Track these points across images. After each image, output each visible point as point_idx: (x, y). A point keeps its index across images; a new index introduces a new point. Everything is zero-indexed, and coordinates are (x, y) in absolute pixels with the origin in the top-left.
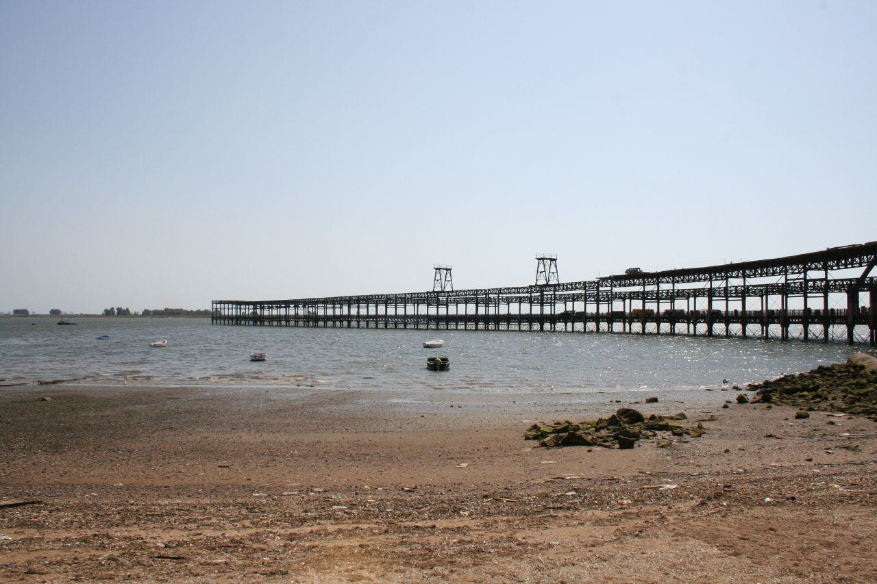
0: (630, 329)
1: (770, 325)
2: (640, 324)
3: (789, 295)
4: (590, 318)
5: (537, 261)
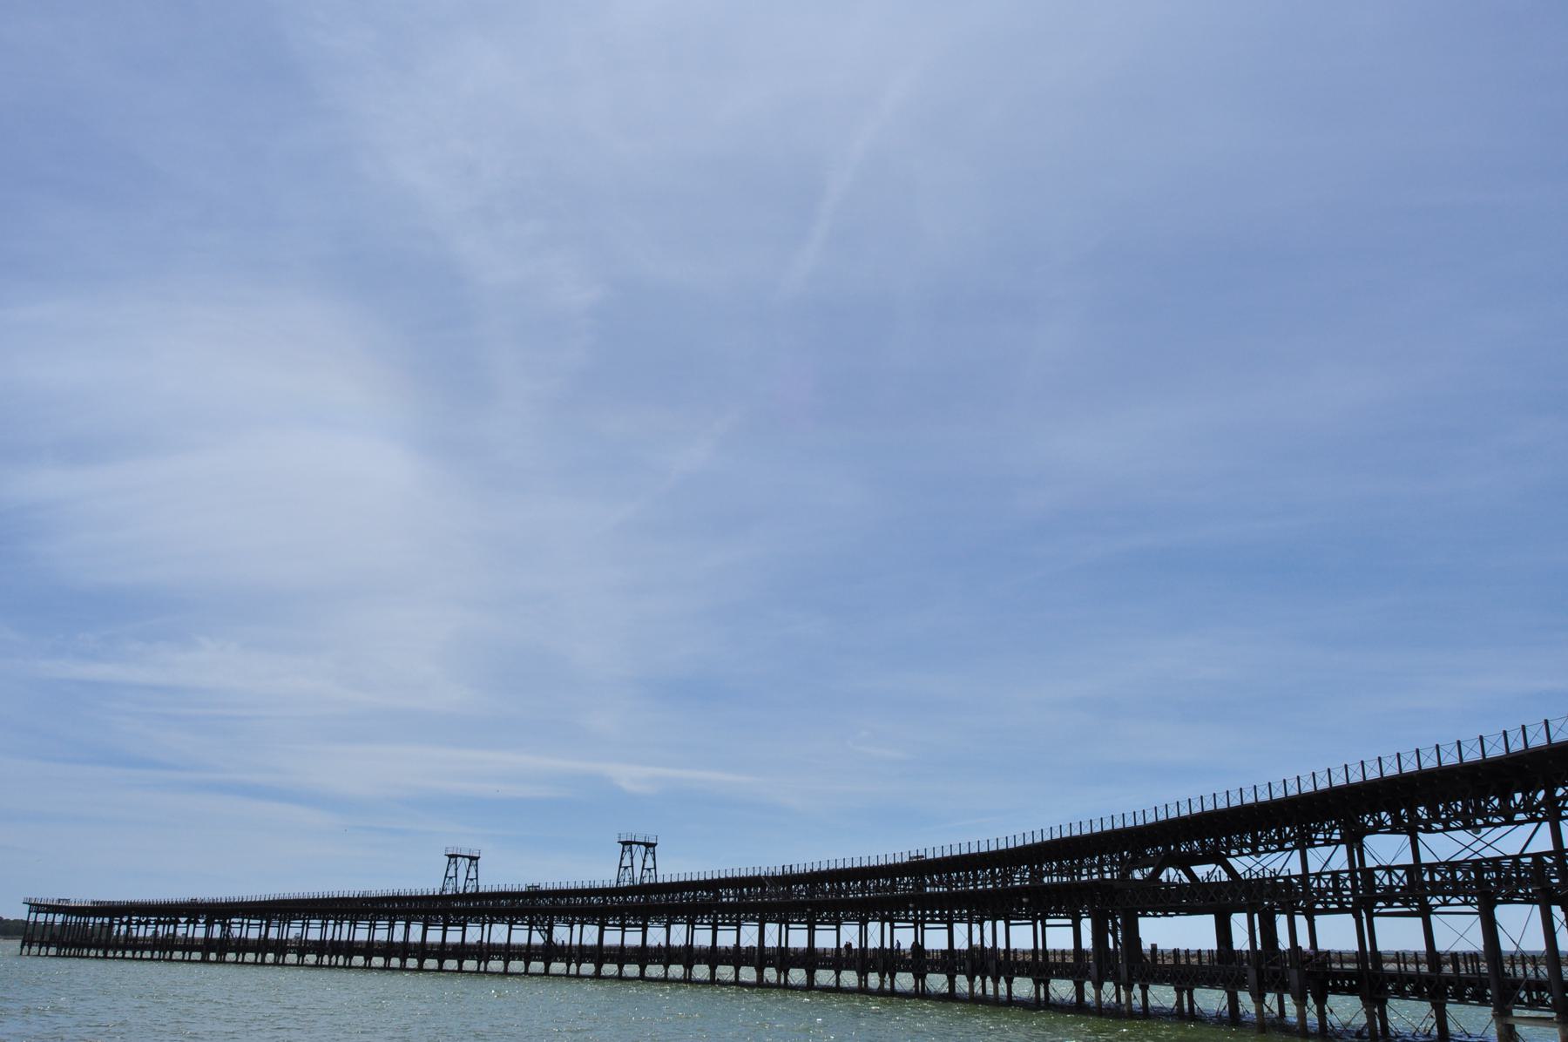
0: (190, 957)
1: (355, 957)
2: (943, 977)
3: (1012, 922)
4: (608, 956)
5: (447, 858)
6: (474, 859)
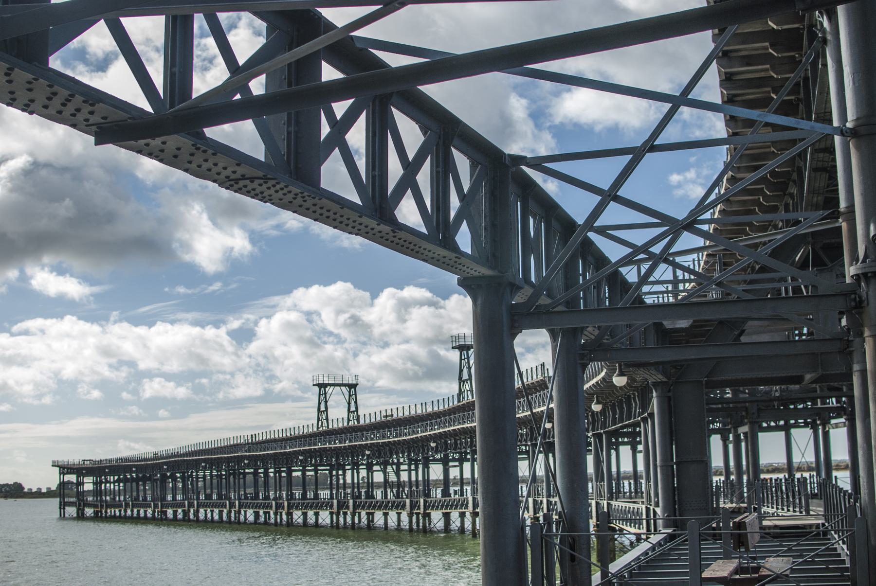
5: (317, 388)
6: (352, 386)
